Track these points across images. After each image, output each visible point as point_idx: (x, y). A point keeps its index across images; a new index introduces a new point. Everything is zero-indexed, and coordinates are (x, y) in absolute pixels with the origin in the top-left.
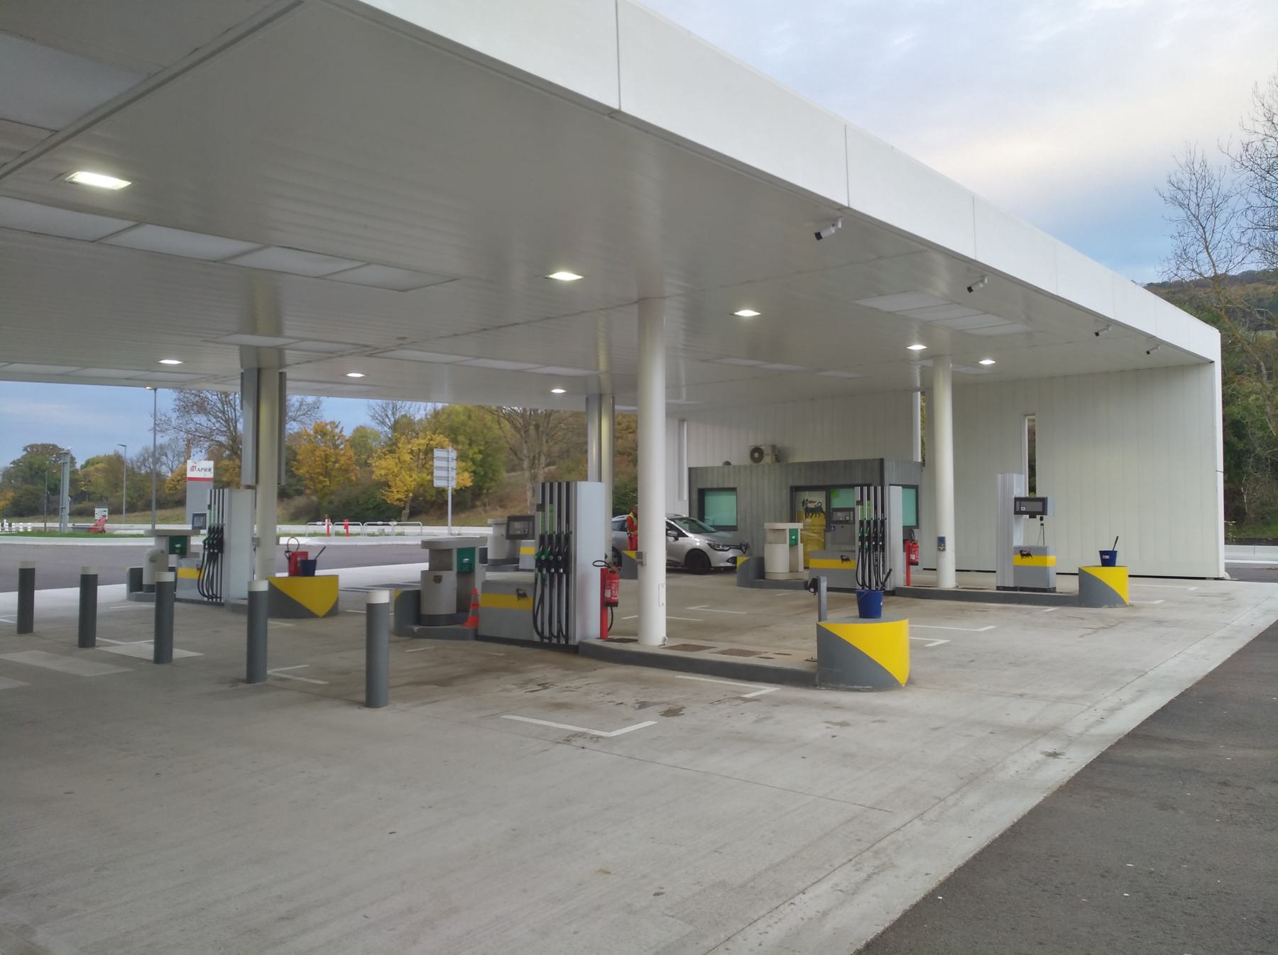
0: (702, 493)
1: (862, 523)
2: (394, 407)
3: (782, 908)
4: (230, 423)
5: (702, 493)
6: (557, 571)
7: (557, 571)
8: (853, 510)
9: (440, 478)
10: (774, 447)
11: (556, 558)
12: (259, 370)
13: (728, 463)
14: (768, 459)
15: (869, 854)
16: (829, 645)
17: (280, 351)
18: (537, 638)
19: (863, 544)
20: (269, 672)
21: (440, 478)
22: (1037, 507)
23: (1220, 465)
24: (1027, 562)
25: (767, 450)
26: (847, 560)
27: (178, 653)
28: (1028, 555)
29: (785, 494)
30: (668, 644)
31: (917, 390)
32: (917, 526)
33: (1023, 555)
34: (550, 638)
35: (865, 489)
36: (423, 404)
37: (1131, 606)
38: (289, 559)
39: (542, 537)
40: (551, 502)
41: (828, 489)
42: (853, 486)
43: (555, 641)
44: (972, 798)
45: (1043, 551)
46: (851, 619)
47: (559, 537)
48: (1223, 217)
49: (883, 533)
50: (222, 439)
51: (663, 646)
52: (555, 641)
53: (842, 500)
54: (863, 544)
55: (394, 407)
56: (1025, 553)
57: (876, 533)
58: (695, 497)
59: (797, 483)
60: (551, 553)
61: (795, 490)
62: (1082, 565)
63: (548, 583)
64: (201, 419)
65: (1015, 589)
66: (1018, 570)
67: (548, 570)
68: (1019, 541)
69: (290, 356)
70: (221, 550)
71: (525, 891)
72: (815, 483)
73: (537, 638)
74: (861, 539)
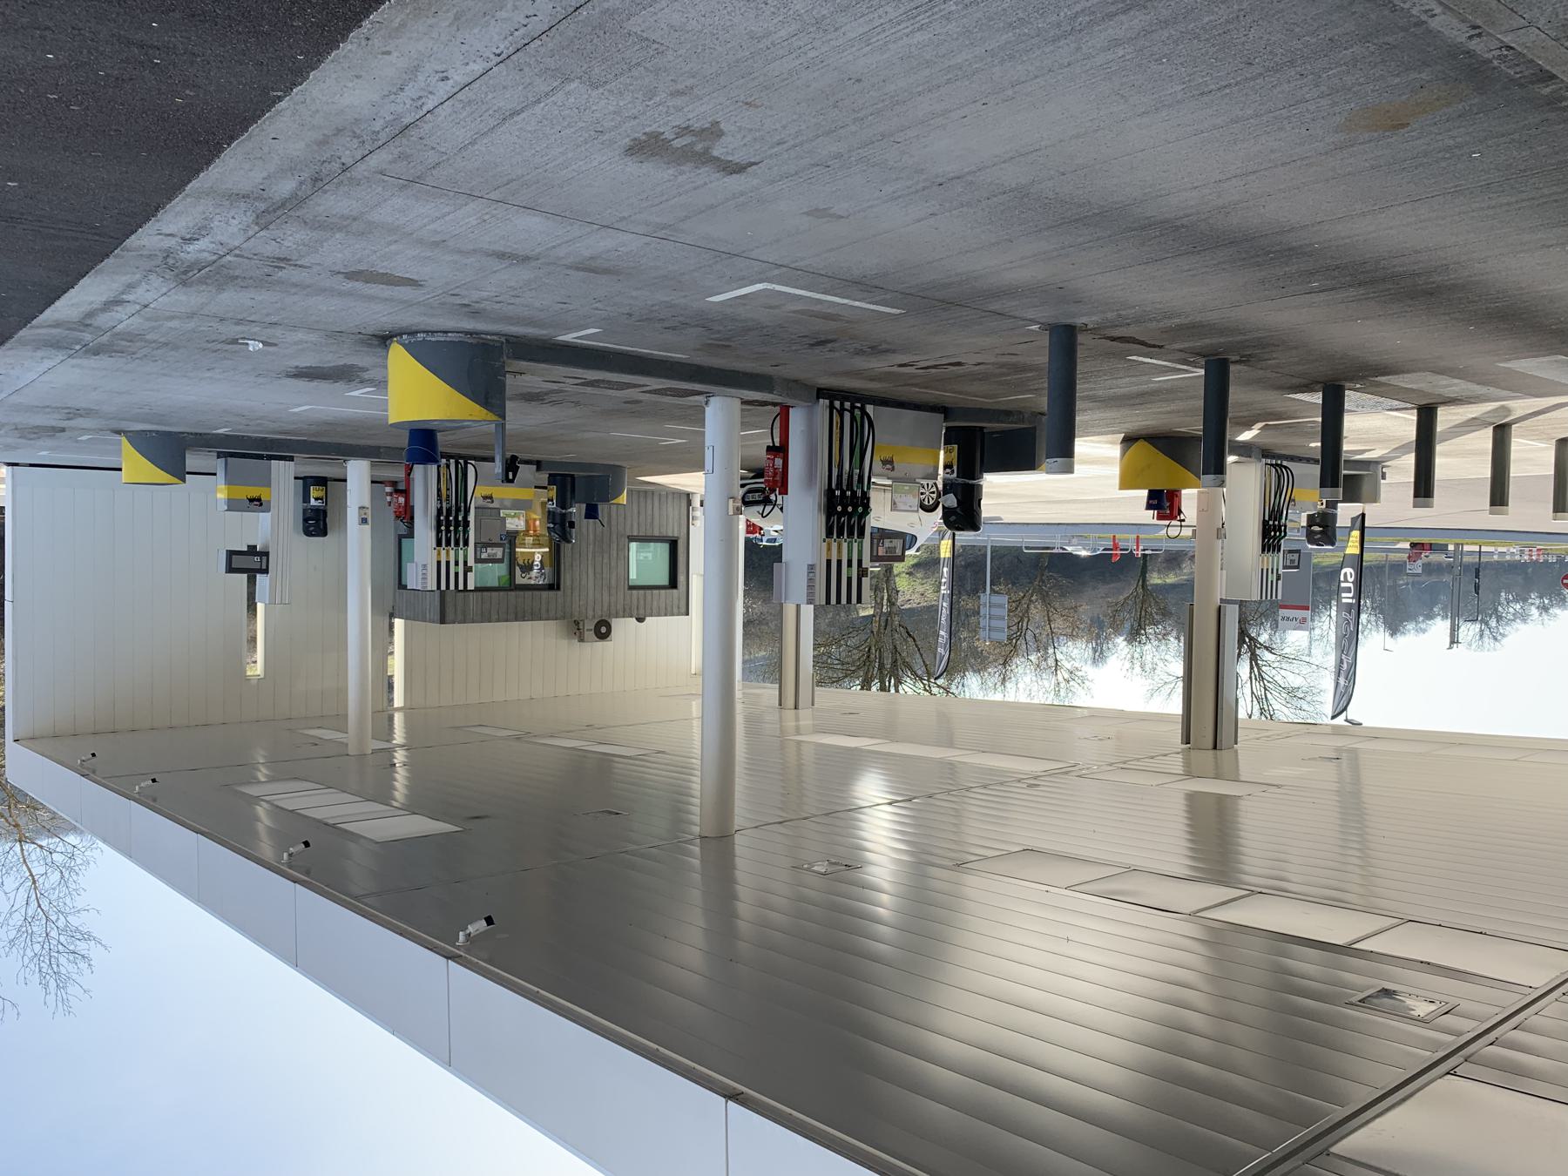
0: (673, 583)
1: (466, 543)
2: (1057, 693)
3: (512, 50)
4: (1257, 674)
5: (673, 583)
6: (843, 492)
7: (843, 492)
8: (477, 561)
9: (1001, 606)
10: (581, 640)
11: (845, 508)
12: (1215, 748)
13: (640, 620)
14: (590, 625)
15: (407, 121)
16: (488, 392)
17: (1189, 773)
18: (870, 409)
19: (456, 517)
20: (1202, 372)
21: (1001, 606)
22: (238, 562)
23: (8, 607)
24: (254, 492)
25: (590, 635)
26: (485, 498)
27: (1317, 398)
28: (251, 500)
29: (566, 580)
30: (701, 398)
31: (398, 709)
32: (400, 538)
33: (259, 500)
34: (853, 407)
35: (461, 587)
36: (1023, 699)
37: (118, 432)
38: (1180, 512)
39: (861, 534)
40: (849, 580)
41: (513, 586)
42: (477, 589)
43: (847, 405)
44: (286, 187)
45: (233, 505)
46: (454, 426)
47: (840, 534)
48: (17, 919)
49: (439, 531)
50: (1267, 656)
51: (709, 395)
52: (847, 405)
53: (495, 574)
54: (456, 517)
55: (1057, 693)
56: (257, 503)
57: (448, 531)
58: (681, 578)
59: (552, 593)
60: (850, 516)
61: (554, 586)
62: (179, 488)
63: (856, 478)
64: (1295, 681)
65: (271, 458)
66: (267, 483)
67: (853, 493)
68: (264, 519)
69: (1176, 764)
70: (1265, 523)
71: (859, 81)
72: (528, 594)
73: (870, 409)
74: (466, 524)
